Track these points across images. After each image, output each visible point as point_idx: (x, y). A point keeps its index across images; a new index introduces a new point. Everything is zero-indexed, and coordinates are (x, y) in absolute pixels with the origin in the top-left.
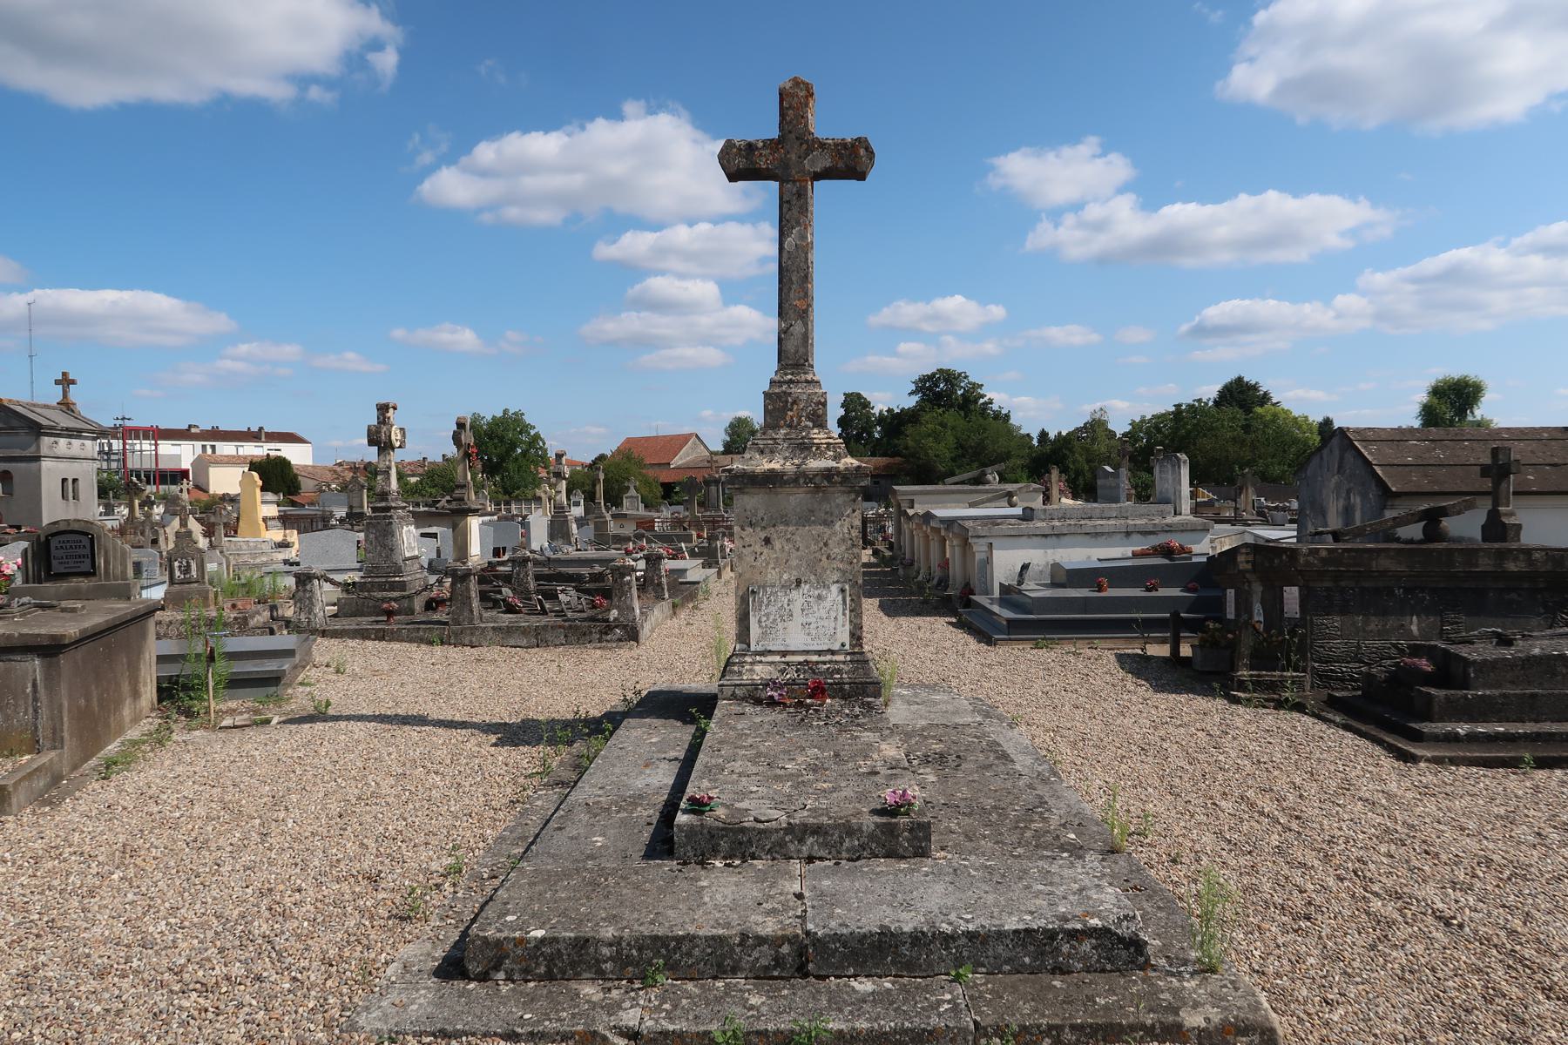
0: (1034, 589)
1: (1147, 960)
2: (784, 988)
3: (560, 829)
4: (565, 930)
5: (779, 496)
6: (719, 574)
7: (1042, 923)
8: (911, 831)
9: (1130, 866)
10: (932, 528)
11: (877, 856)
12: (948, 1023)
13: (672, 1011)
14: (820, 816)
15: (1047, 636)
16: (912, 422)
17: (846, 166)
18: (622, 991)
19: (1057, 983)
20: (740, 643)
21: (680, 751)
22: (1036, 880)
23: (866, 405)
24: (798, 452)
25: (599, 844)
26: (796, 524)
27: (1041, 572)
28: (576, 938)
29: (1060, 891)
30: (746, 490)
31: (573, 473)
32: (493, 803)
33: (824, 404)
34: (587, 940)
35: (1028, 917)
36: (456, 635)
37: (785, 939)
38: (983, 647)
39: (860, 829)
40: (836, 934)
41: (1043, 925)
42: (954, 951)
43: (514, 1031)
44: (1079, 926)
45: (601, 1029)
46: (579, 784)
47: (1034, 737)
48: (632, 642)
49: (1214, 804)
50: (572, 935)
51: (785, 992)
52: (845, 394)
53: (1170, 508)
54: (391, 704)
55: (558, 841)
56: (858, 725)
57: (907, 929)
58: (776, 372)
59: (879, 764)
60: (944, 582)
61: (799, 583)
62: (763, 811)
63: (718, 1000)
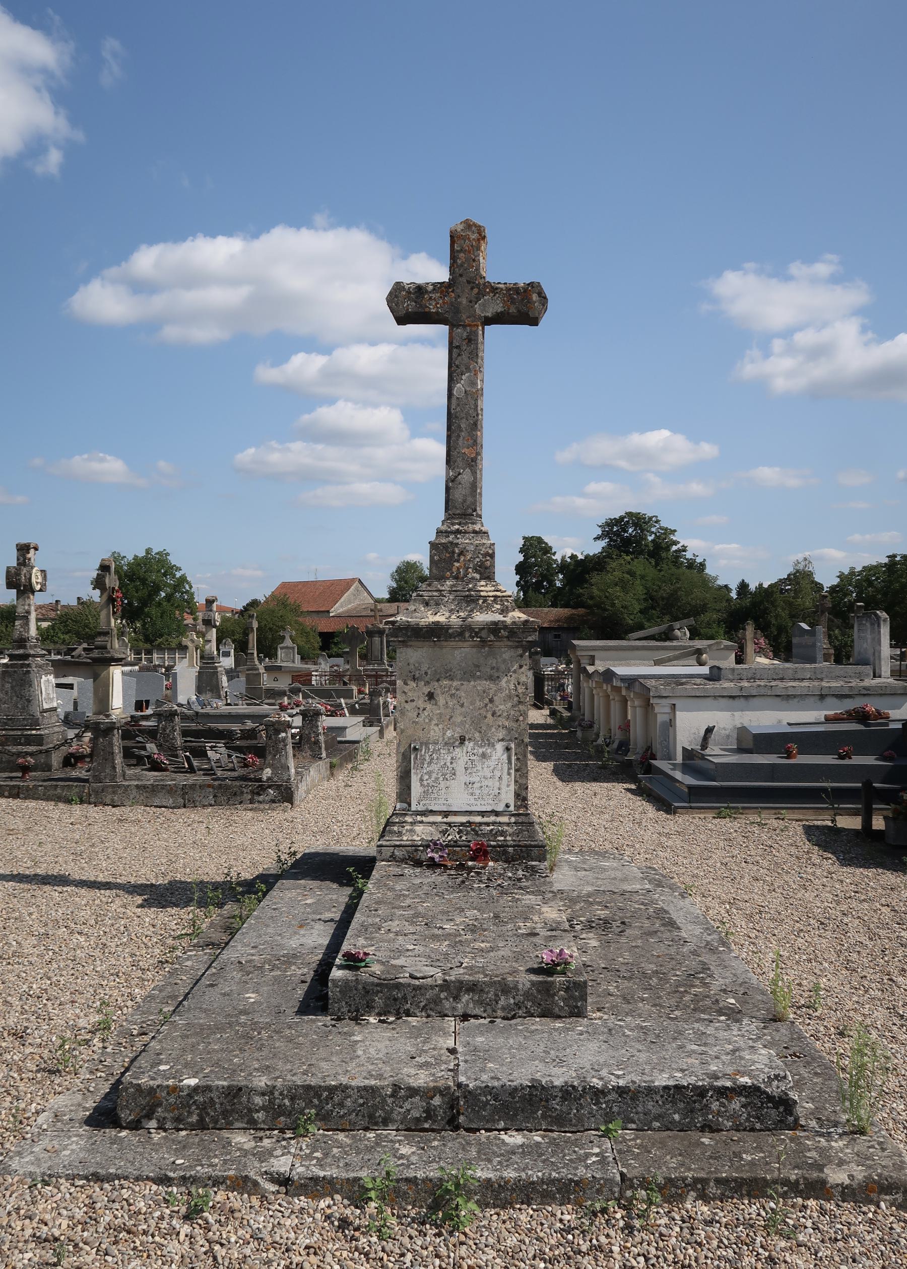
0: (717, 754)
1: (797, 1120)
2: (434, 1139)
3: (212, 985)
4: (219, 1079)
5: (444, 650)
6: (381, 733)
7: (692, 1080)
8: (567, 990)
9: (792, 1034)
10: (613, 687)
11: (532, 1016)
12: (595, 1174)
13: (323, 1159)
14: (477, 973)
15: (731, 805)
16: (597, 570)
17: (519, 311)
18: (274, 1140)
19: (706, 1141)
20: (401, 802)
21: (335, 912)
22: (690, 1040)
23: (547, 550)
24: (464, 605)
25: (252, 1000)
26: (461, 679)
27: (728, 736)
28: (229, 1087)
29: (713, 1051)
30: (410, 643)
31: (224, 620)
32: (141, 963)
33: (492, 556)
34: (240, 1089)
35: (679, 1075)
36: (96, 793)
37: (437, 1091)
38: (662, 815)
39: (516, 988)
40: (487, 1086)
41: (693, 1082)
42: (604, 1106)
43: (166, 1175)
44: (728, 1084)
45: (252, 1174)
46: (232, 943)
47: (708, 908)
48: (286, 804)
49: (891, 980)
50: (225, 1083)
51: (436, 1143)
52: (524, 538)
53: (868, 669)
54: (29, 864)
55: (212, 998)
56: (521, 888)
57: (558, 1083)
58: (443, 522)
59: (539, 925)
60: (624, 746)
61: (462, 740)
62: (418, 968)
63: (369, 1149)
